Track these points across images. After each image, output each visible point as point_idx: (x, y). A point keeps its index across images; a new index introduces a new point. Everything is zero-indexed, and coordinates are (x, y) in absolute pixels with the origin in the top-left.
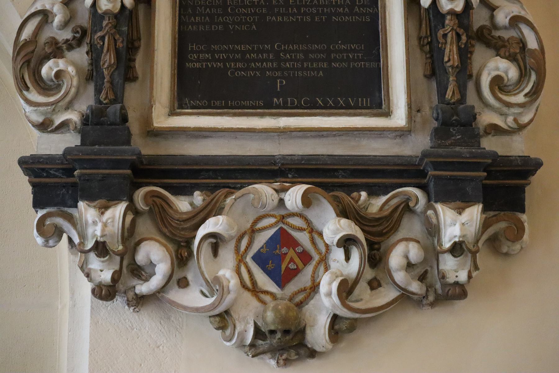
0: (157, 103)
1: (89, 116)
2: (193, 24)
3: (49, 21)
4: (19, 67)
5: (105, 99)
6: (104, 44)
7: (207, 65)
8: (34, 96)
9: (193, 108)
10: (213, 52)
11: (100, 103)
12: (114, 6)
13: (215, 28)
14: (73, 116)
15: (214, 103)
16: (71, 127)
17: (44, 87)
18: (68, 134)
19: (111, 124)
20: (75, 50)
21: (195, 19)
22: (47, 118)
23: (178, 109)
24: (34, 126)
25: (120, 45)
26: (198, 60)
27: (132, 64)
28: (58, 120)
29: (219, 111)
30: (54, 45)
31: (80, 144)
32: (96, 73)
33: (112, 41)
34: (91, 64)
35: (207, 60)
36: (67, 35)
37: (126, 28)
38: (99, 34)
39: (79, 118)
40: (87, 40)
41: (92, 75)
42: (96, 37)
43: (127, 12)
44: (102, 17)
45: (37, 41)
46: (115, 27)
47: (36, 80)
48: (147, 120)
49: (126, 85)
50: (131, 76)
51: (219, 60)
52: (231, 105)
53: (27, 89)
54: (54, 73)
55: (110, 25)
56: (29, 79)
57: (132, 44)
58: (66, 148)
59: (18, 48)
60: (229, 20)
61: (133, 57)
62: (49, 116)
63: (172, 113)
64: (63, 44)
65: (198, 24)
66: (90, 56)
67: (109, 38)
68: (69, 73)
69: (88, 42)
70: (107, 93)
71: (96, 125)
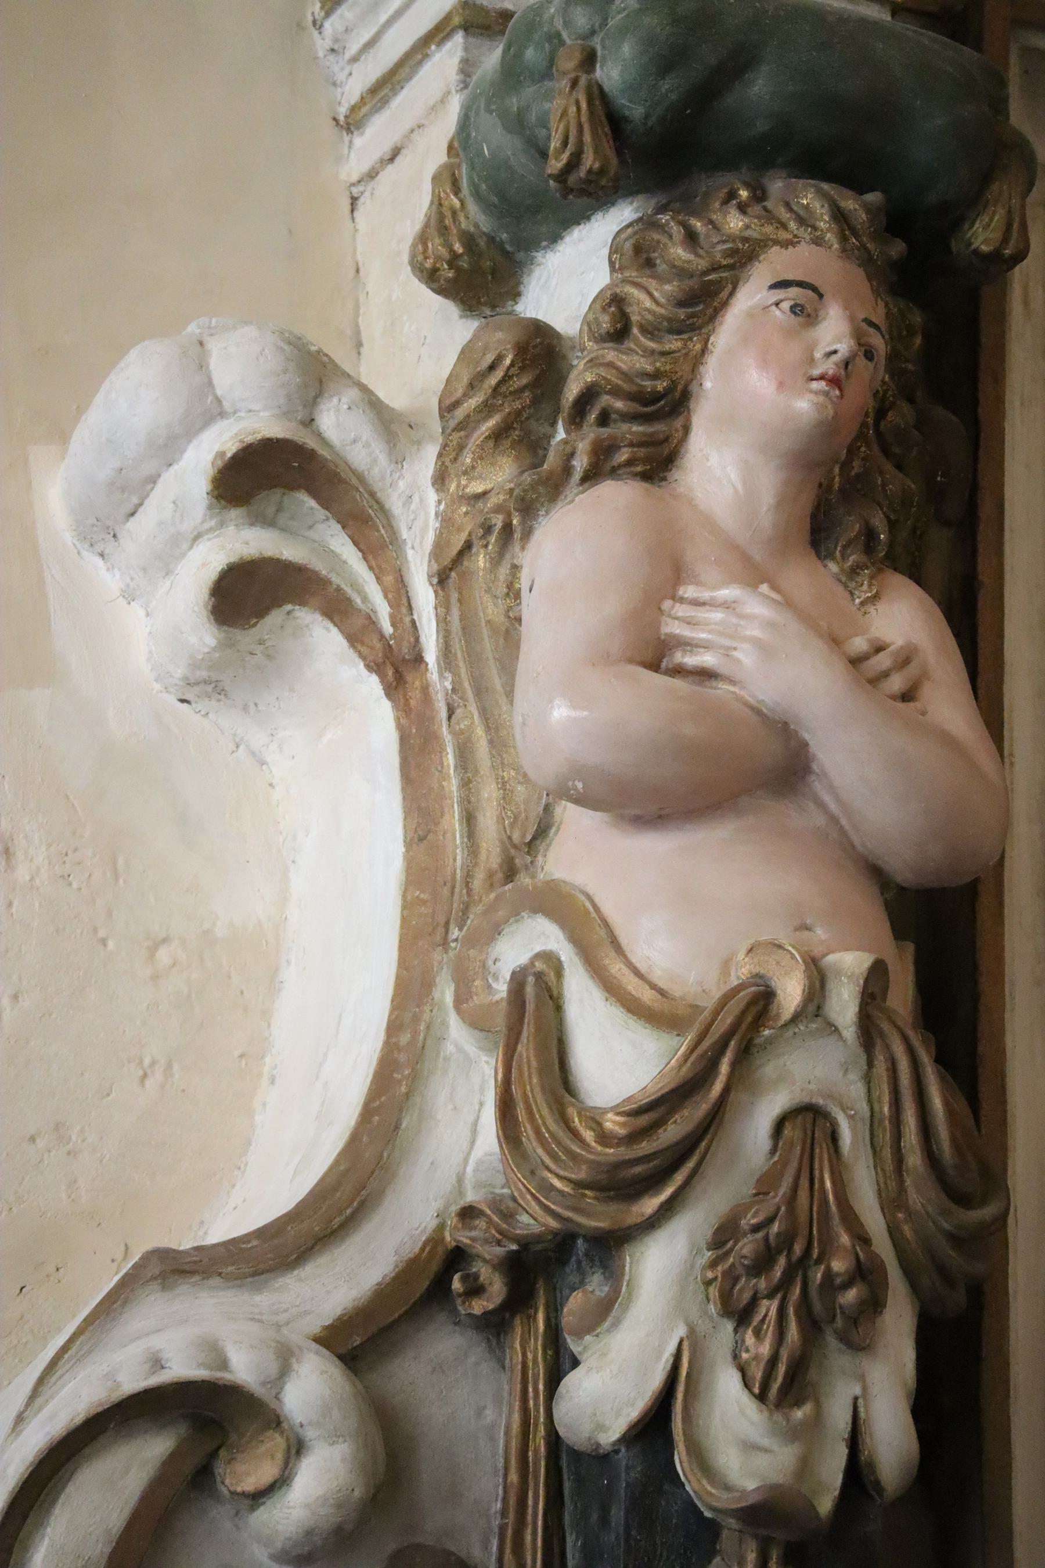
12: (805, 1467)
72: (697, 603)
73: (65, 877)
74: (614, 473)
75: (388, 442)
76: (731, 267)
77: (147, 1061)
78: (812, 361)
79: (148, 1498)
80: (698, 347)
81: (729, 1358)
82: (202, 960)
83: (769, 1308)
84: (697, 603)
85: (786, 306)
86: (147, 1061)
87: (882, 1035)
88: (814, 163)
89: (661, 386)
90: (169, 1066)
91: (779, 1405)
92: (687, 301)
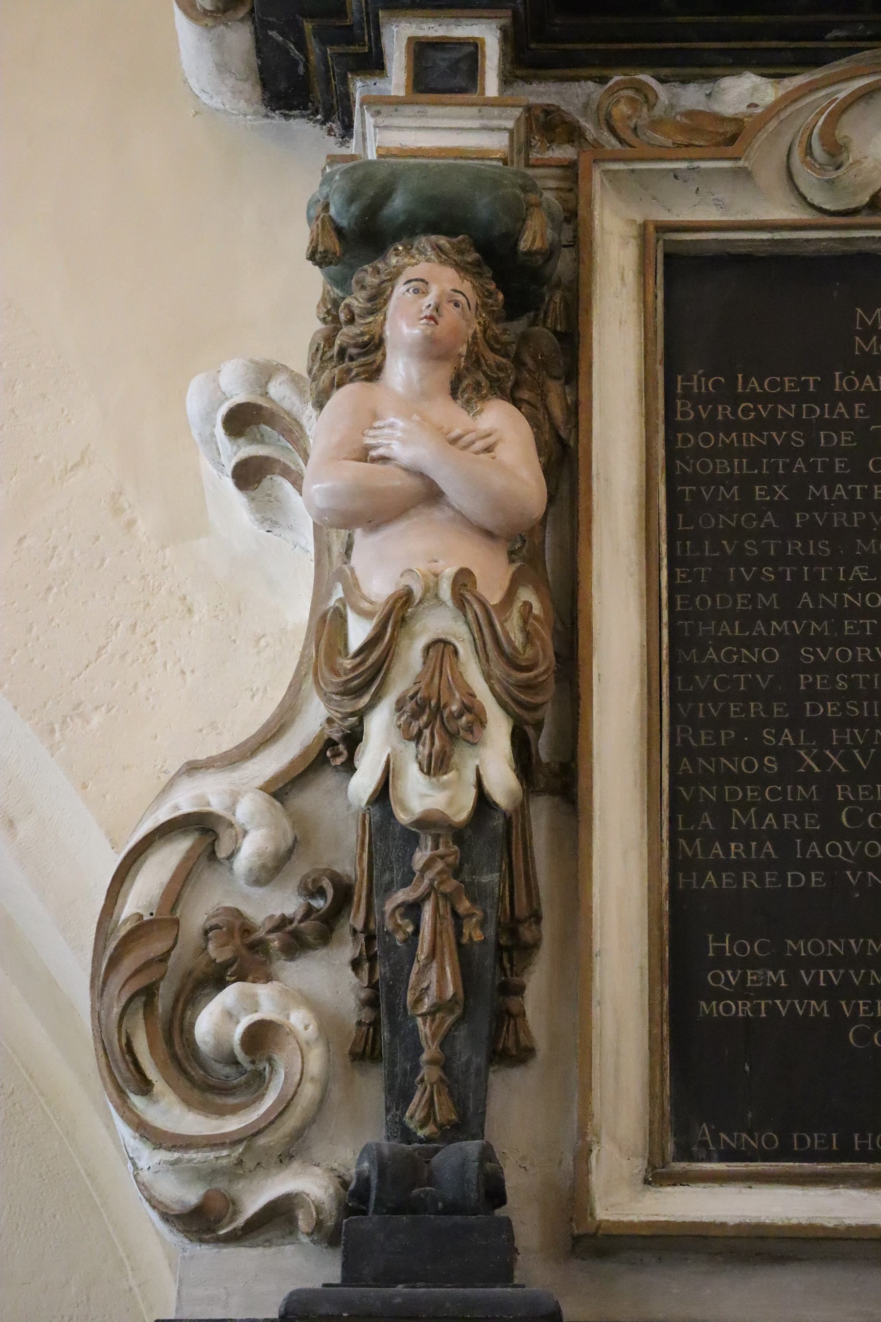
0: (604, 1139)
1: (367, 1180)
2: (719, 866)
3: (222, 854)
4: (116, 1010)
5: (423, 1125)
6: (417, 932)
7: (772, 1010)
8: (170, 1112)
9: (728, 1156)
10: (793, 965)
11: (407, 1135)
12: (451, 802)
13: (796, 880)
14: (310, 1185)
15: (802, 1141)
16: (304, 1222)
17: (210, 1081)
18: (288, 1249)
19: (452, 1209)
20: (311, 953)
21: (727, 852)
22: (218, 1190)
23: (678, 1158)
24: (167, 1217)
25: (473, 933)
26: (742, 992)
27: (512, 1003)
28: (256, 1198)
29: (821, 1167)
30: (237, 935)
31: (338, 1281)
32: (393, 1032)
33: (449, 923)
34: (372, 1003)
35: (774, 992)
36: (284, 902)
37: (496, 876)
38: (402, 896)
39: (331, 1191)
40: (357, 918)
41: (375, 1040)
42: (389, 907)
43: (498, 822)
44: (410, 838)
45: (177, 922)
46: (457, 873)
47: (174, 1057)
48: (573, 1197)
49: (491, 1076)
50: (511, 1043)
51: (814, 992)
52: (863, 1147)
53: (145, 1087)
54: (239, 1031)
55: (440, 865)
56: (152, 1053)
57: (513, 932)
58: (292, 1294)
59: (113, 944)
60: (846, 853)
61: (515, 980)
62: (221, 1184)
63: (657, 1176)
64: (270, 931)
65: (738, 866)
66: (365, 974)
67: (436, 909)
68: (291, 1032)
69: (359, 926)
70: (431, 1102)
71: (398, 1210)
72: (380, 428)
73: (216, 617)
74: (351, 381)
75: (300, 395)
76: (390, 280)
77: (254, 689)
78: (421, 311)
79: (180, 867)
80: (382, 318)
81: (414, 759)
82: (281, 642)
83: (427, 732)
84: (380, 428)
85: (411, 291)
86: (254, 689)
87: (468, 602)
88: (433, 228)
89: (366, 338)
90: (265, 690)
91: (435, 775)
92: (371, 299)
